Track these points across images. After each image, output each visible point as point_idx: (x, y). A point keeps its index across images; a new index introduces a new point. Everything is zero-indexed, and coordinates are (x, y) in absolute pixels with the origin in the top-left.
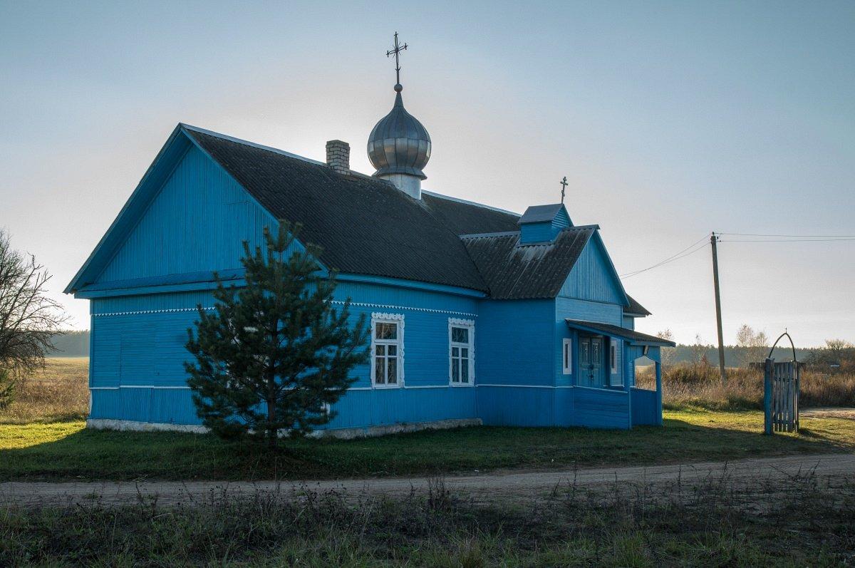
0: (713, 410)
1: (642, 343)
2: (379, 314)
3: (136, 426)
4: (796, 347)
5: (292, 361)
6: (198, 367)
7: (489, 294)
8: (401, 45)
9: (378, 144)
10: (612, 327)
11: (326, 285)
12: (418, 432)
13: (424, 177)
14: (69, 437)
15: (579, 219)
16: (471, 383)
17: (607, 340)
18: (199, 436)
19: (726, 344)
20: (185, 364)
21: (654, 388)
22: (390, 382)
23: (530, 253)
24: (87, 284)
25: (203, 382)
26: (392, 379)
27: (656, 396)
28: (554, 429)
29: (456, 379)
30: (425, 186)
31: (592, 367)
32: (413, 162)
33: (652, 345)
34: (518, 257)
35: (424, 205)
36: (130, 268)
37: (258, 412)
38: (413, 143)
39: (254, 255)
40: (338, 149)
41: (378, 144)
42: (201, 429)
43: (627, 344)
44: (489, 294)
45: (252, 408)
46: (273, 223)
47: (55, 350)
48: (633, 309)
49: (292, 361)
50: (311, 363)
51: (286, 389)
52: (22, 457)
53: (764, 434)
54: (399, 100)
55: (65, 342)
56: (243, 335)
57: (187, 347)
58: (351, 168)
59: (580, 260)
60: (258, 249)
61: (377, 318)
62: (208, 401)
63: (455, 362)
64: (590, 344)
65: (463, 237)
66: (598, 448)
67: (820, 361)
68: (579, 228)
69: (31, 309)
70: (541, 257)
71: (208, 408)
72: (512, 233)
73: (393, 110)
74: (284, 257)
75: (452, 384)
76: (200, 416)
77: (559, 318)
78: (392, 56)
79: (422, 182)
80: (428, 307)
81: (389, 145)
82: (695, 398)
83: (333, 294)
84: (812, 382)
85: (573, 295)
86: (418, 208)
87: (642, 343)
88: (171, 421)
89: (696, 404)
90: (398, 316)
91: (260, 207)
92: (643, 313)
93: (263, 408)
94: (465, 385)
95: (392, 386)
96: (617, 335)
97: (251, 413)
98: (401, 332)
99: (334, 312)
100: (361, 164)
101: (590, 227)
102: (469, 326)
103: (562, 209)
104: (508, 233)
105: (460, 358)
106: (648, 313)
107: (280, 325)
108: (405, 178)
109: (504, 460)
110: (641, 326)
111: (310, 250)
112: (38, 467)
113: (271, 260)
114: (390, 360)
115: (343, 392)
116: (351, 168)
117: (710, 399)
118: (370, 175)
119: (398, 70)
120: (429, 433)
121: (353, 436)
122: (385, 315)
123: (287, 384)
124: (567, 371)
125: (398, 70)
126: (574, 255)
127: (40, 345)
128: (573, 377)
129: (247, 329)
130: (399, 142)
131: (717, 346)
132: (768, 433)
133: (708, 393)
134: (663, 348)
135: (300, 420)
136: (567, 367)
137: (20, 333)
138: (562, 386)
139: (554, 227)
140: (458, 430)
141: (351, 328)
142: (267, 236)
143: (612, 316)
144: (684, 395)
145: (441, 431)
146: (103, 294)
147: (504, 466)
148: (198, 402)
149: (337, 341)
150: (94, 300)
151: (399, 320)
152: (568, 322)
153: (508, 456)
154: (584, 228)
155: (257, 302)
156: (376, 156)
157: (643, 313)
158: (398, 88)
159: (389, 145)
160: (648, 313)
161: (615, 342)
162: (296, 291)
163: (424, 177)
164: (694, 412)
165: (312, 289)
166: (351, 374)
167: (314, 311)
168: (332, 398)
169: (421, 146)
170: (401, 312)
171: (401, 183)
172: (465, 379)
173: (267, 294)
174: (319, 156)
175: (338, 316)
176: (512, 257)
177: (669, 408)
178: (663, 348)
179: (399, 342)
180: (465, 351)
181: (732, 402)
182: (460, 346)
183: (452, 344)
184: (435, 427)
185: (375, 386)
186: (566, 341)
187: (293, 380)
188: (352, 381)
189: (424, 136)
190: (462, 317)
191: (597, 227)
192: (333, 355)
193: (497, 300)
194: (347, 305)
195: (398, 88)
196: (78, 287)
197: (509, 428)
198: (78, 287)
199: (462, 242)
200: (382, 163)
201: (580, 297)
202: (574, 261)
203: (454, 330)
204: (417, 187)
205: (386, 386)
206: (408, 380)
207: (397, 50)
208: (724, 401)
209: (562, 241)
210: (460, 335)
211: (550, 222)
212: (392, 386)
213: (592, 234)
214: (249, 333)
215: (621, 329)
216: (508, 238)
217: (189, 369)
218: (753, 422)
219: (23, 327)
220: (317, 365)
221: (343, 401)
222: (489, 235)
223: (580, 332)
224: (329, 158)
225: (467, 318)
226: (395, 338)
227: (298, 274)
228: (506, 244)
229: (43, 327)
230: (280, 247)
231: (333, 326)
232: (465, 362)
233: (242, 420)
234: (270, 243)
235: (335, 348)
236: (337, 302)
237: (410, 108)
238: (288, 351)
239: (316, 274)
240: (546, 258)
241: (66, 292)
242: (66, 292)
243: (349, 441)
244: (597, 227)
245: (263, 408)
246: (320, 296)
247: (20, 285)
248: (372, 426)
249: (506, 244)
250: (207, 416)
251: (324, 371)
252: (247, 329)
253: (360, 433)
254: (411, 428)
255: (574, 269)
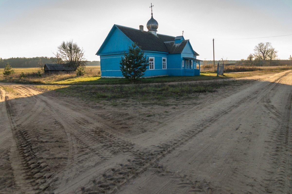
0: (211, 73)
1: (196, 61)
2: (150, 57)
3: (109, 77)
4: (223, 60)
5: (136, 66)
6: (122, 67)
7: (169, 53)
8: (152, 5)
9: (149, 25)
10: (192, 58)
11: (142, 53)
12: (157, 77)
13: (157, 31)
14: (99, 79)
15: (186, 39)
16: (166, 69)
17: (190, 61)
18: (124, 78)
19: (215, 60)
20: (120, 66)
21: (199, 69)
22: (152, 69)
23: (177, 45)
24: (99, 53)
25: (124, 70)
26: (153, 68)
27: (199, 70)
28: (181, 76)
29: (163, 68)
30: (157, 33)
31: (188, 65)
32: (155, 28)
33: (199, 61)
34: (175, 46)
35: (157, 36)
36: (106, 50)
37: (132, 74)
38: (155, 25)
39: (130, 48)
40: (141, 27)
41: (149, 25)
42: (124, 77)
43: (194, 61)
44: (169, 53)
45: (131, 73)
46: (133, 43)
47: (87, 65)
48: (196, 54)
49: (136, 66)
50: (140, 66)
51: (136, 70)
52: (95, 82)
53: (217, 76)
54: (152, 16)
55: (94, 63)
56: (129, 62)
57: (120, 64)
58: (144, 30)
59: (186, 45)
60: (131, 47)
61: (150, 58)
62: (124, 72)
63: (163, 65)
64: (187, 62)
65: (165, 42)
66: (188, 79)
67: (239, 63)
68: (186, 40)
69: (82, 57)
70: (179, 46)
71: (124, 73)
72: (174, 41)
73: (151, 18)
74: (135, 49)
75: (163, 69)
76: (123, 74)
77: (182, 57)
78: (151, 8)
79: (157, 32)
80: (159, 56)
81: (150, 25)
82: (208, 71)
83: (144, 54)
84: (226, 68)
85: (184, 53)
86: (156, 37)
87: (196, 61)
88: (115, 76)
89: (208, 72)
90: (153, 57)
91: (129, 39)
92: (198, 55)
93: (133, 73)
94: (165, 69)
95: (152, 69)
96: (192, 60)
97: (131, 74)
98: (154, 60)
99: (144, 57)
100: (146, 29)
101: (188, 40)
102: (166, 59)
103: (183, 36)
104: (172, 41)
105: (164, 64)
106: (199, 55)
107: (135, 60)
108: (154, 31)
109: (172, 81)
110: (198, 58)
111: (140, 47)
112: (98, 83)
113: (133, 49)
114: (152, 65)
115: (145, 70)
116: (144, 30)
117: (211, 71)
118: (147, 31)
119: (152, 10)
120: (159, 77)
121: (147, 78)
122: (151, 57)
123: (136, 69)
124: (183, 66)
125: (152, 10)
126: (185, 45)
127: (85, 64)
128: (184, 67)
129: (130, 60)
130: (152, 24)
131: (213, 60)
132: (218, 76)
133: (211, 70)
134: (200, 62)
135: (139, 75)
136: (74, 80)
137: (81, 62)
138: (182, 69)
139: (181, 40)
140: (164, 77)
141: (147, 60)
142: (132, 45)
143: (192, 56)
144: (207, 70)
145: (161, 77)
146: (102, 55)
147: (172, 82)
148: (123, 73)
149: (144, 62)
150: (100, 56)
151: (154, 58)
152: (183, 58)
153: (172, 80)
154: (187, 40)
155: (132, 56)
156: (148, 27)
157: (198, 55)
158: (152, 14)
159: (150, 25)
160: (199, 55)
161: (192, 61)
162: (137, 54)
163: (157, 31)
164: (208, 73)
165: (140, 54)
166: (147, 67)
167: (141, 57)
168: (144, 71)
169: (157, 25)
170: (154, 57)
171: (153, 32)
172: (165, 68)
173: (133, 55)
174: (138, 28)
175: (144, 58)
176: (173, 46)
177: (201, 73)
178: (200, 62)
179: (154, 62)
180: (165, 63)
181: (215, 71)
182: (164, 62)
183: (163, 62)
184: (160, 76)
185: (150, 69)
186: (183, 61)
187: (137, 69)
188: (147, 69)
189: (157, 23)
190: (165, 57)
191: (189, 40)
192: (144, 64)
193: (171, 54)
194: (146, 56)
195: (152, 14)
196: (98, 54)
197: (173, 76)
198: (98, 54)
199: (164, 43)
200: (149, 29)
201: (186, 53)
202: (184, 47)
203: (163, 59)
204: (156, 33)
205: (152, 69)
206: (155, 69)
207: (152, 7)
208: (214, 71)
209: (183, 43)
210: (164, 60)
211: (180, 39)
212: (152, 69)
213: (188, 41)
214: (130, 61)
215: (193, 59)
216: (172, 43)
217: (121, 67)
218: (215, 75)
219: (81, 60)
220: (141, 66)
221: (145, 72)
222: (169, 42)
223: (185, 59)
224: (140, 28)
225: (165, 57)
226: (153, 61)
227: (138, 51)
228: (172, 43)
229: (85, 60)
230: (135, 47)
231: (144, 60)
232: (165, 65)
233: (129, 75)
234: (133, 46)
235: (144, 63)
236: (144, 55)
237: (154, 18)
238: (137, 64)
239: (140, 51)
240: (180, 46)
241: (96, 55)
242: (96, 55)
243: (146, 79)
244: (189, 40)
245: (133, 73)
246: (142, 54)
247: (80, 53)
248: (149, 76)
249: (172, 43)
250: (124, 75)
251: (142, 67)
252: (130, 60)
253: (148, 77)
254: (156, 76)
255: (184, 48)
